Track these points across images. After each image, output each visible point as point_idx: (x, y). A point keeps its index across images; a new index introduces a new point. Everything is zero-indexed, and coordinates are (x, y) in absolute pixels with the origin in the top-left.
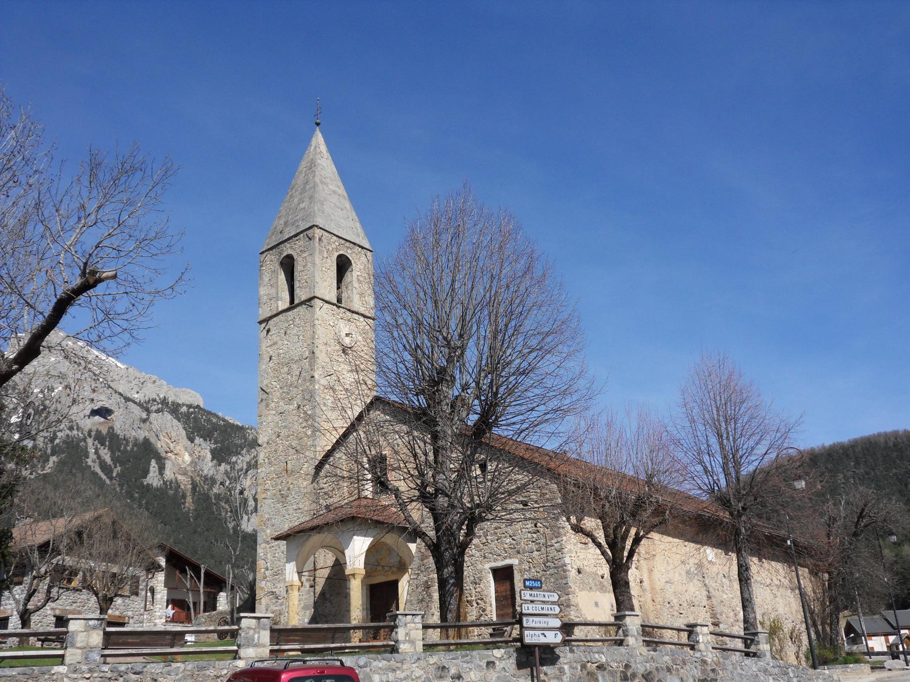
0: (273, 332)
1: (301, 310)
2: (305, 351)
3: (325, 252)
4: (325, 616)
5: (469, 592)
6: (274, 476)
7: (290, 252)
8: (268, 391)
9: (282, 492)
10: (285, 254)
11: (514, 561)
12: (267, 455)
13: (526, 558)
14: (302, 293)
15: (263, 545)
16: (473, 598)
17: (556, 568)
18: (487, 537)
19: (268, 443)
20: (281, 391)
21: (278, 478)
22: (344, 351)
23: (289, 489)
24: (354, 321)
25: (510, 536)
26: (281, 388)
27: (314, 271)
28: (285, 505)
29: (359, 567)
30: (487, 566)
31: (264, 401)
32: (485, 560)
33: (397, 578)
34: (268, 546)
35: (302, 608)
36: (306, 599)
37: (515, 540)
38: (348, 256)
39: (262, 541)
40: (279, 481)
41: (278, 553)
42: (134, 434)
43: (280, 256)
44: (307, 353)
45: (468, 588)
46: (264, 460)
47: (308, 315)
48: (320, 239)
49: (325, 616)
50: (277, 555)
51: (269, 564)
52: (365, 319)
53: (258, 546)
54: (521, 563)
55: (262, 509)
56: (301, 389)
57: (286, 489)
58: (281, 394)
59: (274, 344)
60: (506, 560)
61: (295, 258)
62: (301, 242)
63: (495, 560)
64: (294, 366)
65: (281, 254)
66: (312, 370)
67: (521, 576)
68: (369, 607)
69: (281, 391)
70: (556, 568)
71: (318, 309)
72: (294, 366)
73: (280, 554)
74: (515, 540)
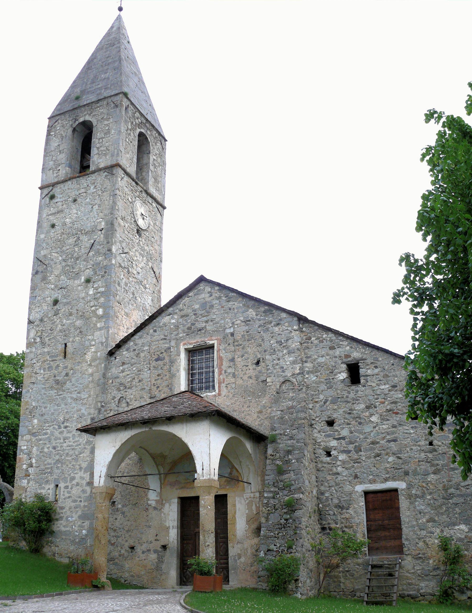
0: (59, 200)
1: (100, 178)
2: (100, 222)
3: (130, 124)
4: (115, 530)
5: (334, 517)
6: (48, 357)
7: (88, 118)
8: (47, 262)
9: (58, 378)
10: (81, 120)
11: (401, 485)
12: (39, 334)
13: (417, 481)
14: (101, 160)
15: (28, 437)
16: (338, 526)
17: (462, 496)
18: (360, 453)
19: (41, 320)
20: (64, 264)
21: (53, 361)
22: (138, 231)
23: (67, 375)
24: (148, 204)
25: (394, 454)
26: (64, 260)
27: (119, 138)
28: (61, 393)
29: (214, 478)
30: (360, 488)
31: (39, 273)
32: (356, 480)
33: (226, 493)
34: (34, 439)
35: (79, 517)
36: (85, 506)
37: (400, 458)
38: (148, 136)
39: (26, 432)
40: (54, 365)
41: (48, 448)
42: (96, 159)
43: (75, 122)
44: (103, 223)
45: (331, 512)
46: (35, 339)
47: (108, 184)
48: (126, 109)
49: (115, 530)
50: (46, 450)
51: (34, 461)
52: (158, 206)
53: (20, 438)
54: (410, 486)
55: (28, 395)
56: (92, 263)
57: (64, 373)
58: (63, 267)
59: (58, 212)
60: (387, 483)
61: (94, 125)
62: (102, 110)
63: (372, 482)
64: (84, 238)
65: (76, 120)
66: (108, 243)
67: (410, 503)
68: (179, 526)
69: (64, 264)
70: (462, 496)
71: (119, 179)
72: (84, 238)
73: (51, 449)
74: (400, 458)
